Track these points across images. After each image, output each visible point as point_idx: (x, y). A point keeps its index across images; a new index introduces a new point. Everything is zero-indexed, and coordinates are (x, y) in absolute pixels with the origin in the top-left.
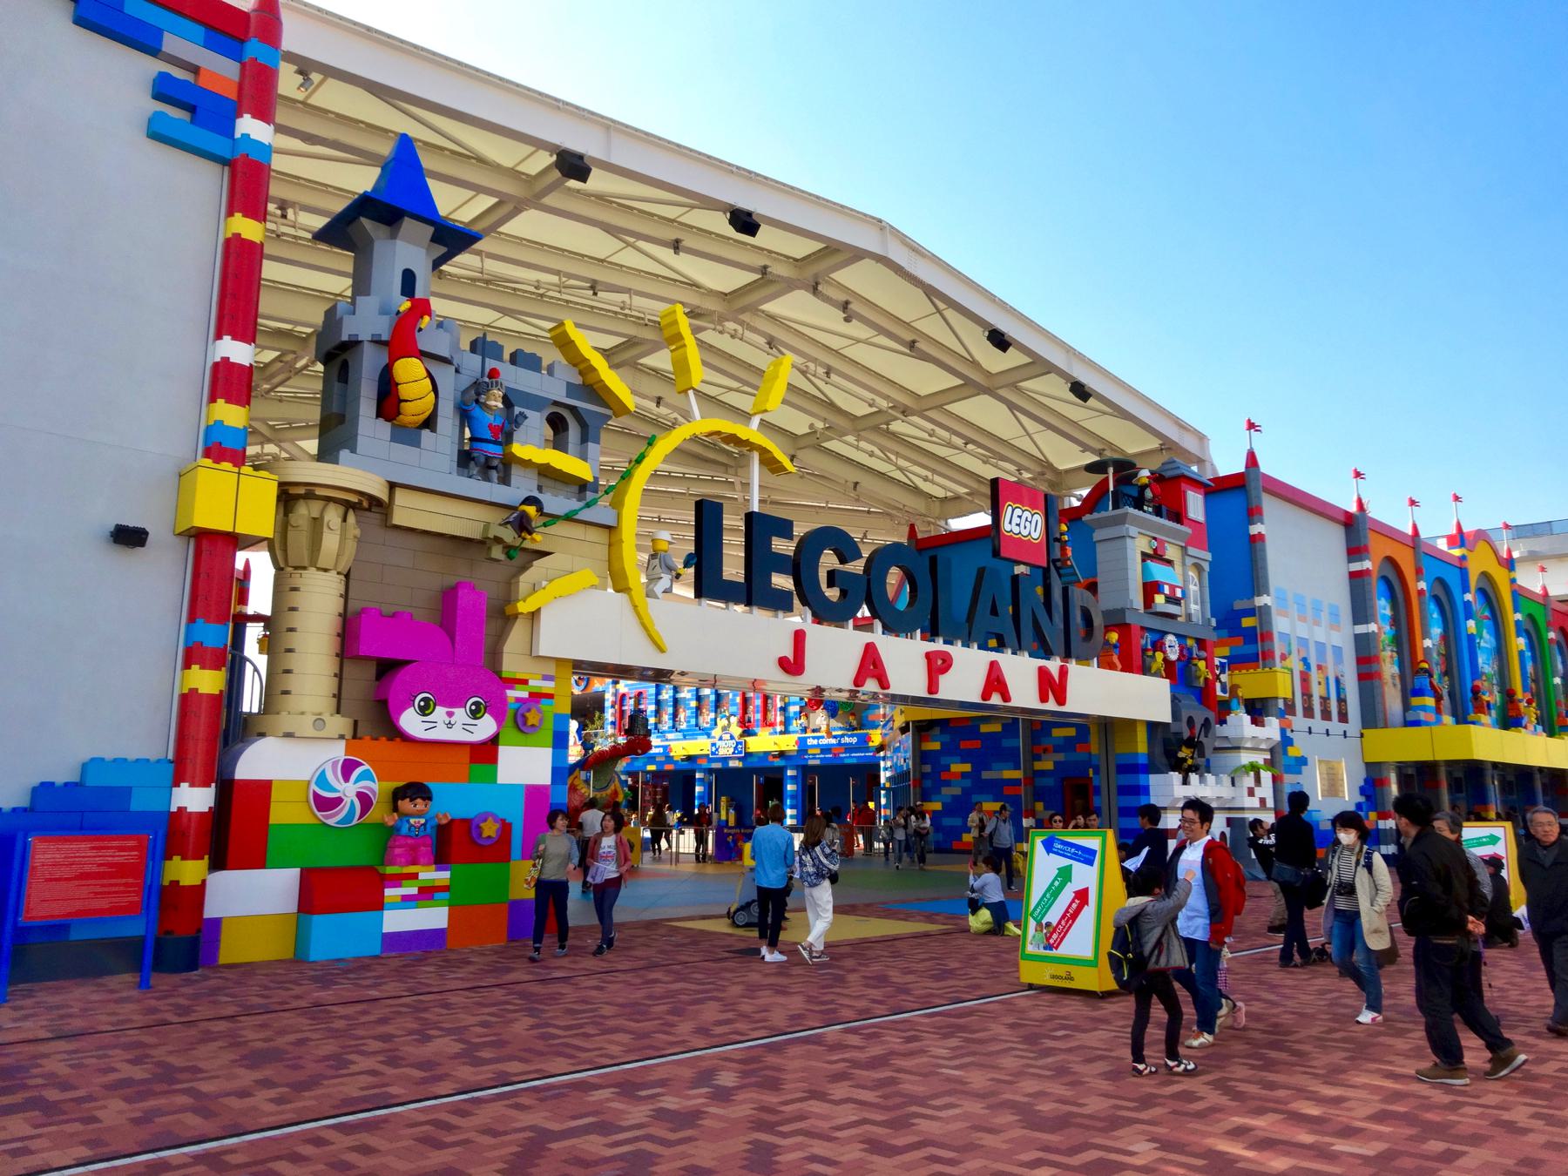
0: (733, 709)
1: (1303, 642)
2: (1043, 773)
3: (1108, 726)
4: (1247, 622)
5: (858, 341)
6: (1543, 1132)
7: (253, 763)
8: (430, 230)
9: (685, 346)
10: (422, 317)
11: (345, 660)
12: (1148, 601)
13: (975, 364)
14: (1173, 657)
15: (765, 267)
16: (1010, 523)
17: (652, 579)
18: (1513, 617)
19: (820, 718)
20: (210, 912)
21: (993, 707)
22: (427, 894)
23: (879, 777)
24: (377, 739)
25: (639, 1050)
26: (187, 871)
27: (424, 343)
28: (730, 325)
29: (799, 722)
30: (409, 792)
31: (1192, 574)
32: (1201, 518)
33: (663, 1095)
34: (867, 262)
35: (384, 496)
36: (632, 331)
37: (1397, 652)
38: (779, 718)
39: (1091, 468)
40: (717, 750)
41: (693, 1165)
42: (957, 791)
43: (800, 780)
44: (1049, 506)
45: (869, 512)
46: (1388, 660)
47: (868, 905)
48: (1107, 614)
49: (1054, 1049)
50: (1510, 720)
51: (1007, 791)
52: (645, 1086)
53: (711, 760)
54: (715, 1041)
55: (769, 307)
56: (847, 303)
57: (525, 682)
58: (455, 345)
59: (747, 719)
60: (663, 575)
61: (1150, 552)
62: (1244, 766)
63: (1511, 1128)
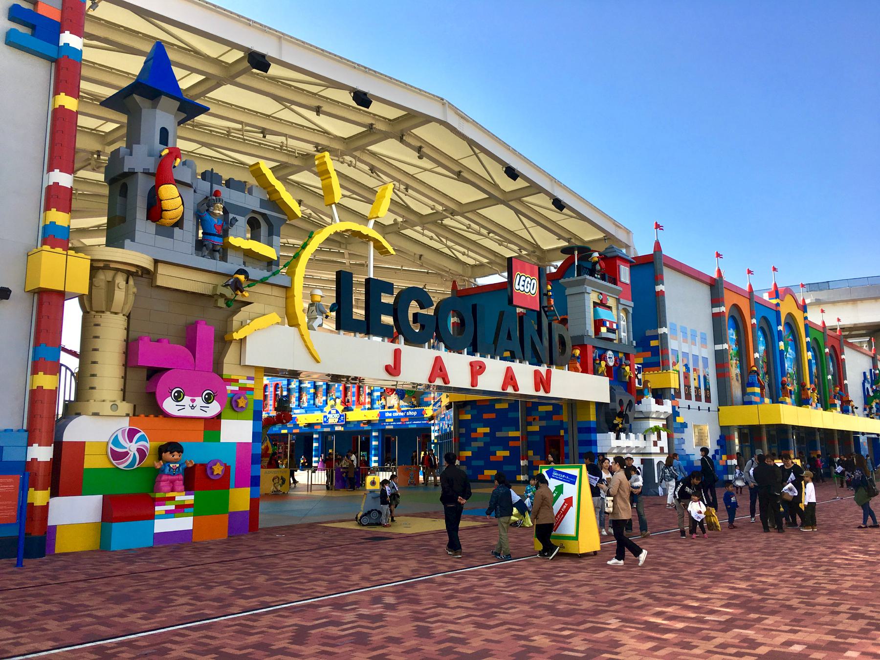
0: (338, 394)
1: (685, 355)
2: (533, 433)
3: (574, 405)
4: (653, 343)
5: (426, 170)
6: (804, 609)
7: (73, 433)
8: (178, 104)
9: (330, 177)
10: (175, 159)
11: (128, 368)
12: (597, 331)
13: (496, 186)
14: (611, 364)
15: (372, 125)
16: (519, 285)
17: (311, 319)
18: (805, 340)
19: (393, 400)
20: (51, 522)
21: (507, 394)
22: (180, 509)
23: (431, 436)
24: (147, 416)
25: (335, 588)
26: (38, 497)
27: (177, 175)
28: (348, 158)
29: (380, 402)
30: (169, 449)
31: (622, 314)
32: (628, 282)
33: (358, 608)
34: (433, 124)
35: (151, 268)
36: (284, 159)
37: (739, 361)
38: (368, 400)
39: (564, 250)
40: (327, 420)
41: (389, 637)
42: (481, 444)
43: (380, 439)
44: (542, 276)
45: (428, 273)
46: (734, 365)
47: (435, 513)
48: (573, 338)
49: (561, 581)
50: (802, 401)
51: (511, 444)
52: (347, 604)
53: (323, 427)
54: (374, 583)
55: (372, 148)
56: (421, 147)
57: (237, 381)
58: (194, 174)
59: (346, 400)
60: (318, 316)
61: (598, 301)
62: (651, 428)
63: (790, 607)
